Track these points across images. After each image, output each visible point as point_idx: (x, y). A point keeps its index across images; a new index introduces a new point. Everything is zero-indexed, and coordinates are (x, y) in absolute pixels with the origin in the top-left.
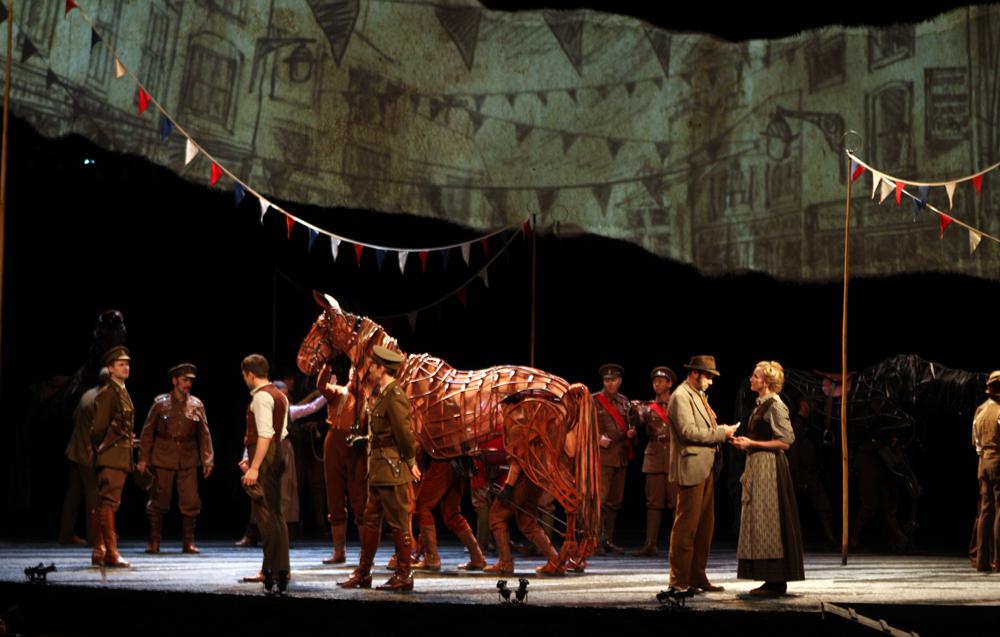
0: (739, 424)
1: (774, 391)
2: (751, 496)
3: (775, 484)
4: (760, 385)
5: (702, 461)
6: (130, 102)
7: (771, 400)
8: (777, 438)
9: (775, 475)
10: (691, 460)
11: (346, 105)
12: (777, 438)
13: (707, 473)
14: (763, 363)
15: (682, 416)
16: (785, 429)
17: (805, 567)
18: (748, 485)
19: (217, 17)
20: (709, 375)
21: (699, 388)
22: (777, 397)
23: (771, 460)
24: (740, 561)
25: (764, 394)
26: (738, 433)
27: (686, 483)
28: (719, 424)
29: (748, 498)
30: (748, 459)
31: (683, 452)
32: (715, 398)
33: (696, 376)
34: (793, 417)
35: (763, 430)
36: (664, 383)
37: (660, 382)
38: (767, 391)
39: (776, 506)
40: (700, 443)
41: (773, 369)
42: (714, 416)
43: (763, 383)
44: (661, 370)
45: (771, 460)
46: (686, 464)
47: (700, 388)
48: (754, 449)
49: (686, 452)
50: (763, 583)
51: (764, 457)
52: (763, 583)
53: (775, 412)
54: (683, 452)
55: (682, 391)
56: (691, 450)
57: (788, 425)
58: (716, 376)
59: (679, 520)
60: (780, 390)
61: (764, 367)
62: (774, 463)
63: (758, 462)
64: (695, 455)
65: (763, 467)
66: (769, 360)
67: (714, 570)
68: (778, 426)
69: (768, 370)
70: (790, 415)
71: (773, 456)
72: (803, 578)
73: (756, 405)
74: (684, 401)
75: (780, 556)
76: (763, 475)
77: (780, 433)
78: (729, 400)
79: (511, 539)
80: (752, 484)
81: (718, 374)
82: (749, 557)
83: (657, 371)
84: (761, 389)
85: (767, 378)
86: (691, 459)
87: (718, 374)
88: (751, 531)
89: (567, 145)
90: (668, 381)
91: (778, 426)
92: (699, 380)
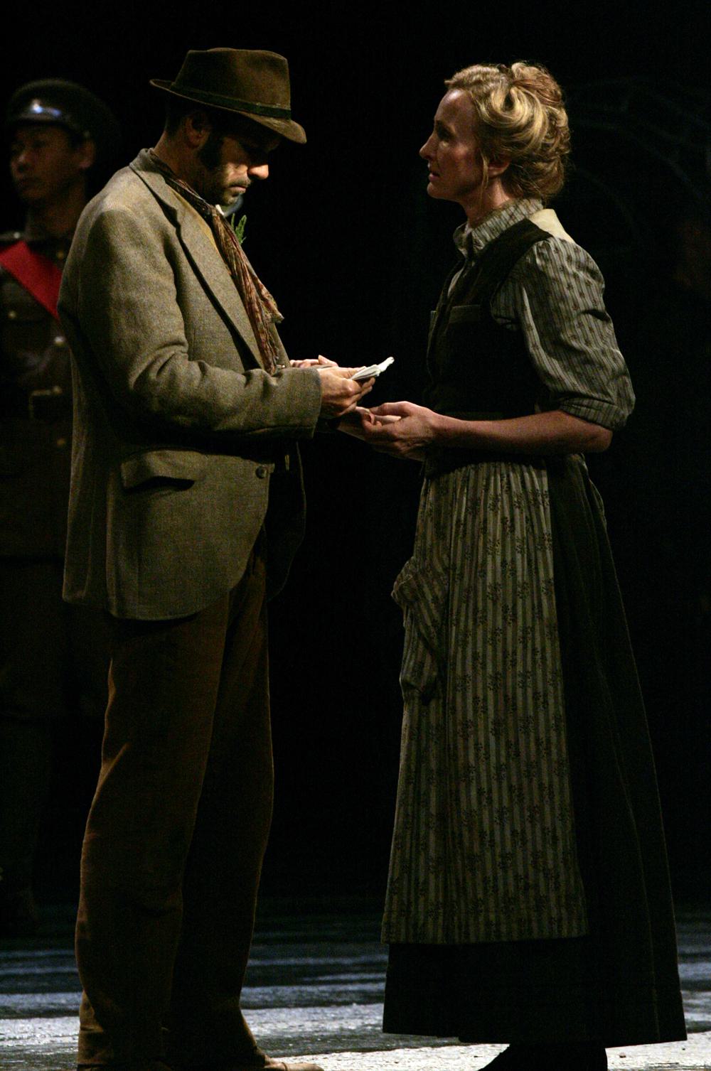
0: (390, 361)
1: (529, 195)
2: (443, 663)
3: (548, 607)
4: (466, 173)
5: (219, 503)
6: (103, 210)
7: (528, 234)
8: (560, 400)
9: (547, 571)
10: (165, 504)
11: (401, 430)
12: (560, 400)
13: (235, 561)
14: (475, 71)
15: (131, 306)
16: (587, 360)
17: (686, 971)
18: (429, 613)
19: (186, 210)
20: (258, 145)
21: (205, 192)
22: (547, 220)
23: (531, 501)
24: (395, 950)
25: (488, 209)
26: (378, 393)
27: (141, 611)
28: (297, 352)
29: (429, 671)
30: (428, 499)
31: (126, 470)
32: (274, 239)
33: (201, 138)
34: (619, 307)
35: (482, 362)
36: (55, 147)
37: (38, 146)
38: (500, 197)
39: (555, 706)
40: (202, 428)
41: (526, 101)
42: (271, 311)
43: (475, 159)
44: (47, 97)
45: (531, 501)
46: (138, 533)
47: (215, 193)
48: (446, 453)
49: (143, 469)
50: (508, 1045)
51: (497, 484)
52: (508, 1045)
53: (541, 284)
54: (126, 470)
55: (129, 195)
56: (161, 463)
57: (602, 343)
58: (287, 145)
59: (110, 776)
60: (542, 207)
61: (479, 93)
62: (545, 513)
63: (474, 503)
64: (183, 485)
65: (495, 527)
66: (503, 60)
67: (286, 991)
68: (559, 348)
69: (497, 101)
70: (607, 295)
71: (541, 482)
72: (676, 1031)
73: (455, 261)
74: (140, 242)
75: (572, 929)
76: (497, 548)
77: (570, 381)
78: (348, 245)
79: (236, 213)
80: (445, 606)
81: (298, 133)
82: (434, 932)
83: (27, 102)
84: (468, 189)
85: (496, 136)
86: (166, 502)
87: (298, 133)
88: (442, 817)
89: (547, 874)
90: (75, 141)
91: (559, 348)
92: (213, 161)
